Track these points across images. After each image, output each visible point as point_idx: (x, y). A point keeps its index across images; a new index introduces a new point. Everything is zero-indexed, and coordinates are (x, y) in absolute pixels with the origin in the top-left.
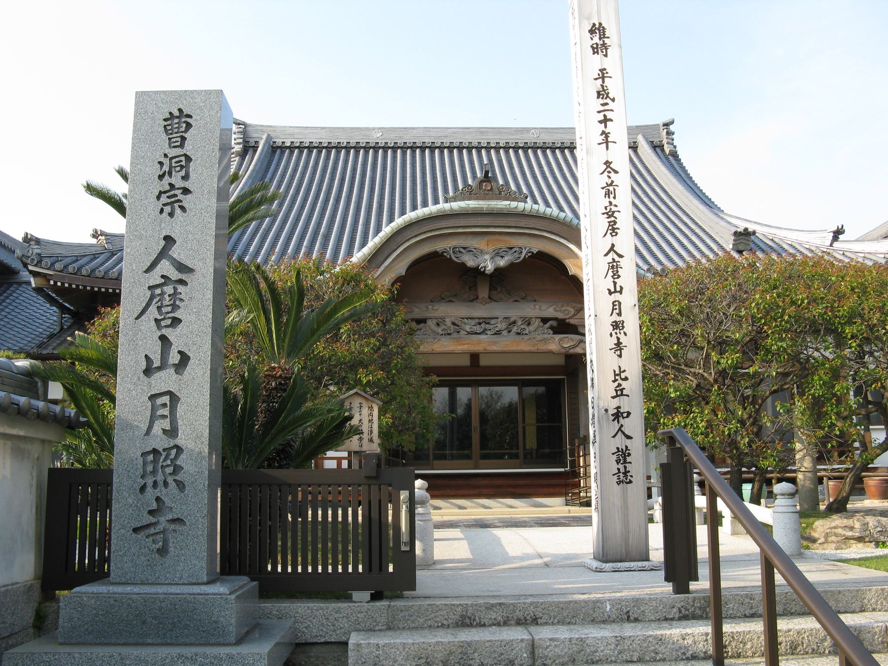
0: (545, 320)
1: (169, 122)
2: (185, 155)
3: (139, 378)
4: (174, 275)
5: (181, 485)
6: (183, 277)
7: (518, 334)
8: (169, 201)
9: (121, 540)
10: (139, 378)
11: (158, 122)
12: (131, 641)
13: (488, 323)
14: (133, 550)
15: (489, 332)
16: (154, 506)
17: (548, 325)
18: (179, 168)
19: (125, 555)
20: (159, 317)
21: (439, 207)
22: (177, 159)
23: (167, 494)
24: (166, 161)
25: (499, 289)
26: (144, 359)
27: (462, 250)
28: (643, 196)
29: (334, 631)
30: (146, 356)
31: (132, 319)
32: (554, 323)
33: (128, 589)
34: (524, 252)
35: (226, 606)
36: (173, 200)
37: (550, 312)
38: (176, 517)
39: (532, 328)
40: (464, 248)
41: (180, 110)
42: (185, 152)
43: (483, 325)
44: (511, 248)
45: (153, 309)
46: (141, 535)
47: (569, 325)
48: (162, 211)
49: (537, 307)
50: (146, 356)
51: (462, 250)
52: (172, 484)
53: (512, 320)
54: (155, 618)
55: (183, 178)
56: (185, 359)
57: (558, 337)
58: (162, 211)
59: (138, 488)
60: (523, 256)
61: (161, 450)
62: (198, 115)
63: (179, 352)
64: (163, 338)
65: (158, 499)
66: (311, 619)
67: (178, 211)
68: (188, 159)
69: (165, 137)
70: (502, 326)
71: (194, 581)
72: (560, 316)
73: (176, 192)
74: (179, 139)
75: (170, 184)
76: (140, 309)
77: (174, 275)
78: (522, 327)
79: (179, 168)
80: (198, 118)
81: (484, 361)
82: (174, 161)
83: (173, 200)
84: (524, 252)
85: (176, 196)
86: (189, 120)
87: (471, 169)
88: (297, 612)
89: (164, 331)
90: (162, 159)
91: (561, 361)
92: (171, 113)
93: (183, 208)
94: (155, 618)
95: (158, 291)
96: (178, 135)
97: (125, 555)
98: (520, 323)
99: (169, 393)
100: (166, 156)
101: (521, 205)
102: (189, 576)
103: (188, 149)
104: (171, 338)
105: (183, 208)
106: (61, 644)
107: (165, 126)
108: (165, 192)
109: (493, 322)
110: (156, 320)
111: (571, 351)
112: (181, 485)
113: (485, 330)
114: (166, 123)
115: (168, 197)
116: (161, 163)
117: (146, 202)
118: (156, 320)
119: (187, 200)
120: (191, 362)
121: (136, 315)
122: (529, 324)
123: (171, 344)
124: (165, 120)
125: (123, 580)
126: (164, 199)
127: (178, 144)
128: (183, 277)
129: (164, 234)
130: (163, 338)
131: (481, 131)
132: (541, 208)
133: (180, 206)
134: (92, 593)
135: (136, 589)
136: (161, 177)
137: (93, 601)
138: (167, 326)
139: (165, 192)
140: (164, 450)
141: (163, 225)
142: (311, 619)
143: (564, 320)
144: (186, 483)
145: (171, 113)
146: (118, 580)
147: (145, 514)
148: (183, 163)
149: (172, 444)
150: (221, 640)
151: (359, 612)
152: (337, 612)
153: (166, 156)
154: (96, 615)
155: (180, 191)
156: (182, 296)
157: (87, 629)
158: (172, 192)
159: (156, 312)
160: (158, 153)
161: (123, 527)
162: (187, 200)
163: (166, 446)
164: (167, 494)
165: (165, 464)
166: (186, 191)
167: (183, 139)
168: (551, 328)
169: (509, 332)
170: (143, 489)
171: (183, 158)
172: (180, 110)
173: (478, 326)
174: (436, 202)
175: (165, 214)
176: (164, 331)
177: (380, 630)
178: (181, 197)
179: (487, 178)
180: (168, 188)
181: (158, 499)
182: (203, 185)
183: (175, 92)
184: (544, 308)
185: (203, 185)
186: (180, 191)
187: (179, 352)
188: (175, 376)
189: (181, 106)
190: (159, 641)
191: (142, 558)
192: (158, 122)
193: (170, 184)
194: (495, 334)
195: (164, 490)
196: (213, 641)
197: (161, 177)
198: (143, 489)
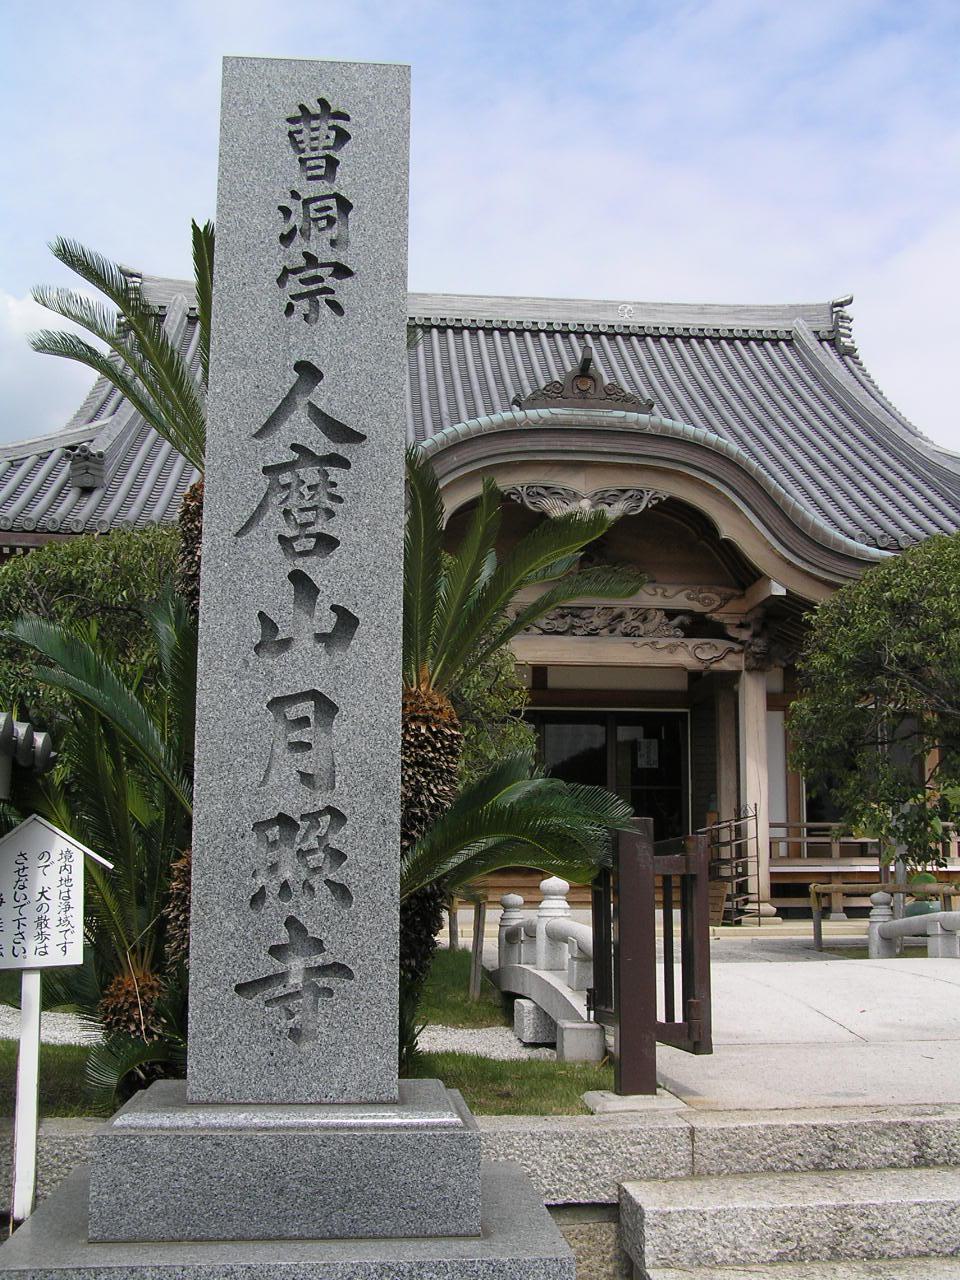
0: (671, 614)
1: (297, 127)
2: (336, 196)
3: (246, 662)
4: (321, 444)
5: (342, 892)
6: (342, 450)
7: (627, 635)
8: (305, 289)
9: (211, 1010)
10: (246, 662)
11: (274, 125)
12: (253, 1232)
13: (577, 616)
14: (237, 1032)
15: (578, 632)
16: (283, 936)
17: (676, 621)
18: (323, 223)
19: (219, 1042)
20: (290, 533)
21: (496, 418)
22: (319, 204)
23: (311, 912)
24: (296, 207)
25: (596, 560)
26: (256, 621)
27: (542, 491)
28: (811, 417)
29: (584, 1182)
30: (261, 615)
31: (228, 535)
32: (687, 620)
33: (241, 1118)
34: (646, 498)
35: (463, 1153)
36: (313, 287)
37: (680, 600)
38: (330, 960)
39: (650, 626)
40: (546, 488)
41: (323, 102)
42: (336, 189)
43: (568, 619)
44: (624, 491)
45: (273, 514)
46: (256, 1000)
47: (710, 622)
48: (290, 309)
49: (659, 591)
50: (261, 615)
51: (542, 491)
52: (323, 891)
53: (616, 612)
54: (305, 1181)
55: (333, 243)
56: (347, 623)
57: (692, 642)
58: (290, 309)
59: (247, 899)
60: (643, 506)
61: (296, 817)
62: (362, 114)
63: (334, 608)
64: (299, 579)
65: (291, 923)
66: (538, 1157)
67: (325, 310)
68: (345, 206)
69: (291, 155)
70: (597, 622)
71: (371, 1096)
72: (697, 607)
73: (320, 272)
74: (323, 163)
75: (306, 255)
76: (247, 515)
77: (321, 444)
78: (634, 623)
79: (323, 223)
80: (362, 120)
81: (554, 681)
82: (313, 206)
83: (313, 287)
84: (646, 498)
85: (320, 279)
86: (341, 123)
87: (556, 362)
88: (511, 1146)
89: (300, 564)
90: (287, 202)
91: (681, 684)
92: (302, 108)
93: (336, 307)
94: (305, 1181)
95: (286, 478)
96: (321, 153)
97: (219, 1042)
98: (630, 616)
99: (314, 695)
100: (295, 195)
101: (644, 418)
102: (361, 1088)
103: (343, 183)
104: (317, 579)
105: (336, 307)
106: (92, 1242)
107: (291, 134)
108: (295, 271)
109: (585, 614)
110: (282, 539)
111: (715, 666)
112: (342, 892)
113: (573, 627)
114: (293, 128)
115: (301, 281)
116: (286, 212)
117: (254, 289)
118: (282, 539)
119: (344, 290)
120: (361, 629)
121: (236, 528)
122: (645, 620)
123: (318, 591)
124: (291, 120)
125: (216, 1096)
126: (294, 285)
127: (321, 172)
128: (342, 450)
129: (296, 358)
130: (299, 579)
131: (537, 303)
132: (679, 425)
133: (328, 302)
134: (161, 1128)
135: (259, 1118)
136: (286, 239)
137: (166, 1147)
138: (305, 554)
139: (295, 271)
140: (303, 817)
141: (293, 339)
142: (538, 1157)
143: (702, 615)
144: (352, 889)
145: (302, 108)
146: (204, 1097)
147: (264, 955)
148: (334, 213)
149: (321, 805)
150: (452, 1227)
151: (634, 1143)
152: (588, 1144)
153: (295, 195)
154: (175, 1176)
155: (330, 270)
156: (338, 491)
157: (154, 1208)
158: (312, 272)
159: (283, 522)
160: (278, 189)
161: (215, 982)
162: (344, 290)
163: (308, 809)
164: (311, 912)
165: (305, 847)
166: (341, 271)
167: (332, 163)
168: (681, 626)
169: (612, 631)
170: (258, 899)
171: (332, 203)
172: (323, 102)
173: (561, 621)
174: (491, 410)
175: (296, 317)
176: (300, 564)
177: (675, 1178)
178: (330, 282)
179: (585, 369)
180: (302, 262)
181: (291, 923)
182: (377, 261)
183: (311, 63)
184: (670, 591)
185: (377, 261)
186: (330, 270)
187: (334, 608)
188: (324, 661)
189: (324, 95)
190: (315, 1231)
191: (258, 1048)
192: (274, 125)
193: (306, 255)
194: (589, 634)
195: (304, 901)
196: (435, 1229)
197: (286, 239)
198: (258, 899)
